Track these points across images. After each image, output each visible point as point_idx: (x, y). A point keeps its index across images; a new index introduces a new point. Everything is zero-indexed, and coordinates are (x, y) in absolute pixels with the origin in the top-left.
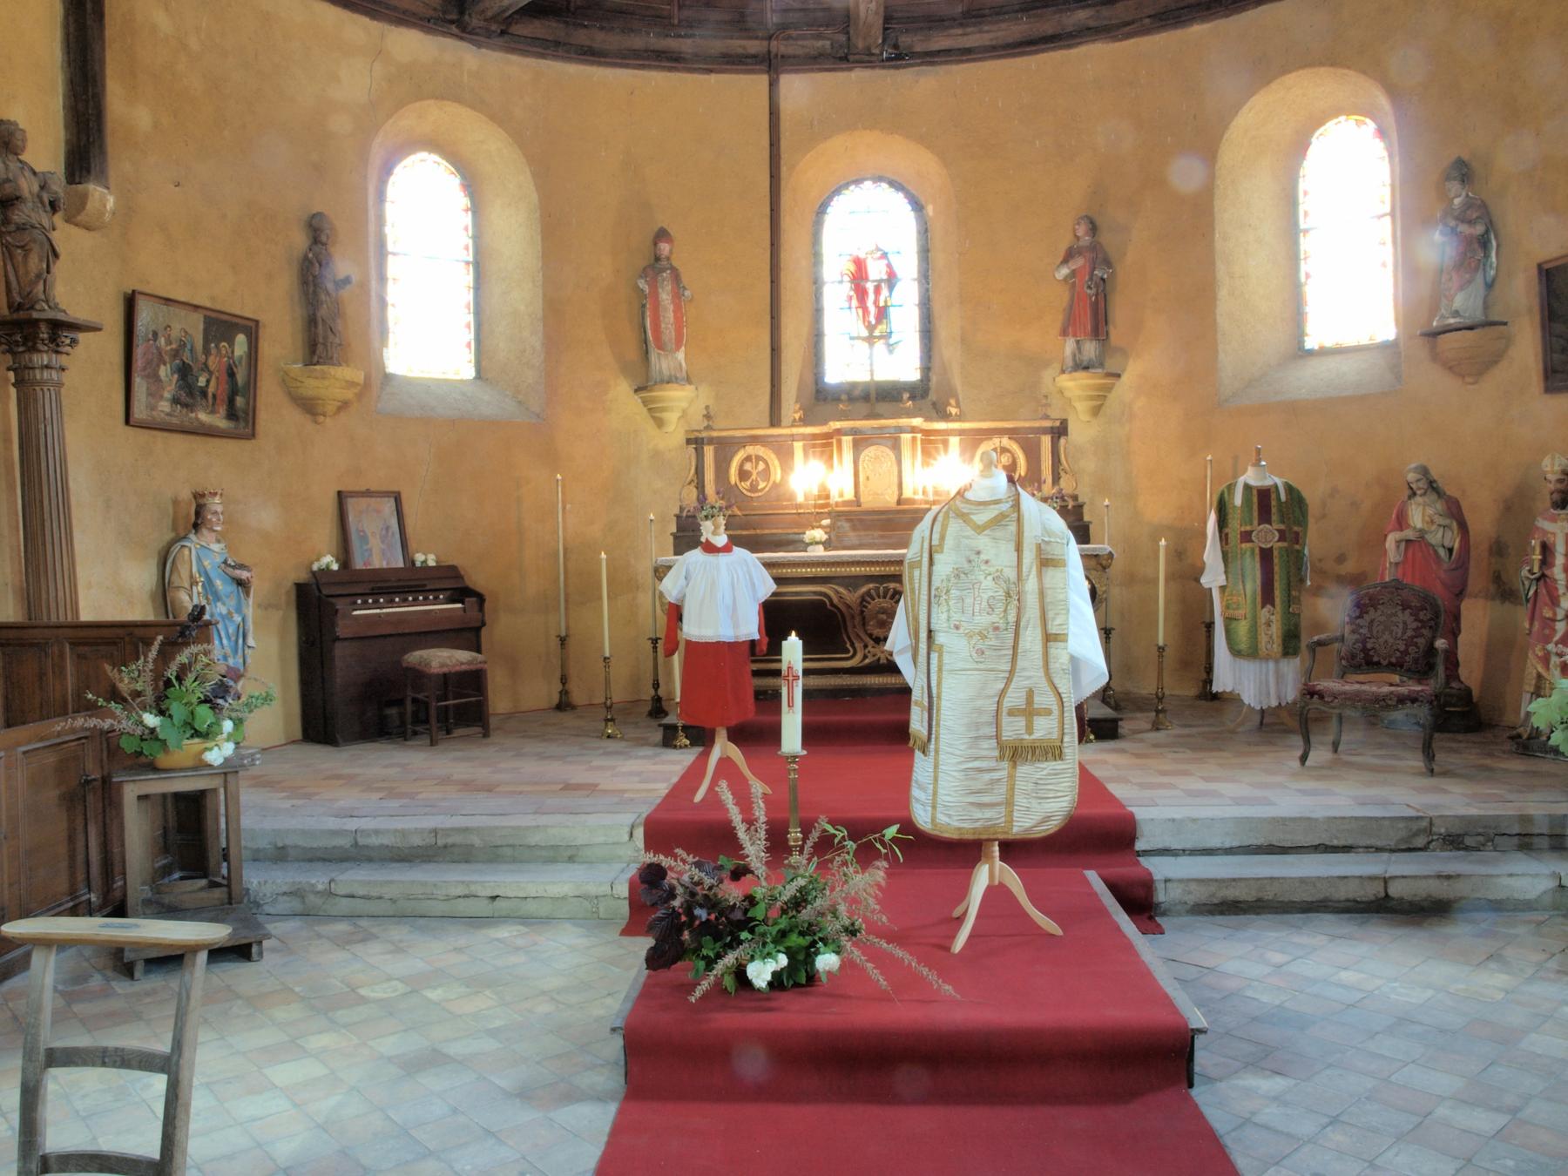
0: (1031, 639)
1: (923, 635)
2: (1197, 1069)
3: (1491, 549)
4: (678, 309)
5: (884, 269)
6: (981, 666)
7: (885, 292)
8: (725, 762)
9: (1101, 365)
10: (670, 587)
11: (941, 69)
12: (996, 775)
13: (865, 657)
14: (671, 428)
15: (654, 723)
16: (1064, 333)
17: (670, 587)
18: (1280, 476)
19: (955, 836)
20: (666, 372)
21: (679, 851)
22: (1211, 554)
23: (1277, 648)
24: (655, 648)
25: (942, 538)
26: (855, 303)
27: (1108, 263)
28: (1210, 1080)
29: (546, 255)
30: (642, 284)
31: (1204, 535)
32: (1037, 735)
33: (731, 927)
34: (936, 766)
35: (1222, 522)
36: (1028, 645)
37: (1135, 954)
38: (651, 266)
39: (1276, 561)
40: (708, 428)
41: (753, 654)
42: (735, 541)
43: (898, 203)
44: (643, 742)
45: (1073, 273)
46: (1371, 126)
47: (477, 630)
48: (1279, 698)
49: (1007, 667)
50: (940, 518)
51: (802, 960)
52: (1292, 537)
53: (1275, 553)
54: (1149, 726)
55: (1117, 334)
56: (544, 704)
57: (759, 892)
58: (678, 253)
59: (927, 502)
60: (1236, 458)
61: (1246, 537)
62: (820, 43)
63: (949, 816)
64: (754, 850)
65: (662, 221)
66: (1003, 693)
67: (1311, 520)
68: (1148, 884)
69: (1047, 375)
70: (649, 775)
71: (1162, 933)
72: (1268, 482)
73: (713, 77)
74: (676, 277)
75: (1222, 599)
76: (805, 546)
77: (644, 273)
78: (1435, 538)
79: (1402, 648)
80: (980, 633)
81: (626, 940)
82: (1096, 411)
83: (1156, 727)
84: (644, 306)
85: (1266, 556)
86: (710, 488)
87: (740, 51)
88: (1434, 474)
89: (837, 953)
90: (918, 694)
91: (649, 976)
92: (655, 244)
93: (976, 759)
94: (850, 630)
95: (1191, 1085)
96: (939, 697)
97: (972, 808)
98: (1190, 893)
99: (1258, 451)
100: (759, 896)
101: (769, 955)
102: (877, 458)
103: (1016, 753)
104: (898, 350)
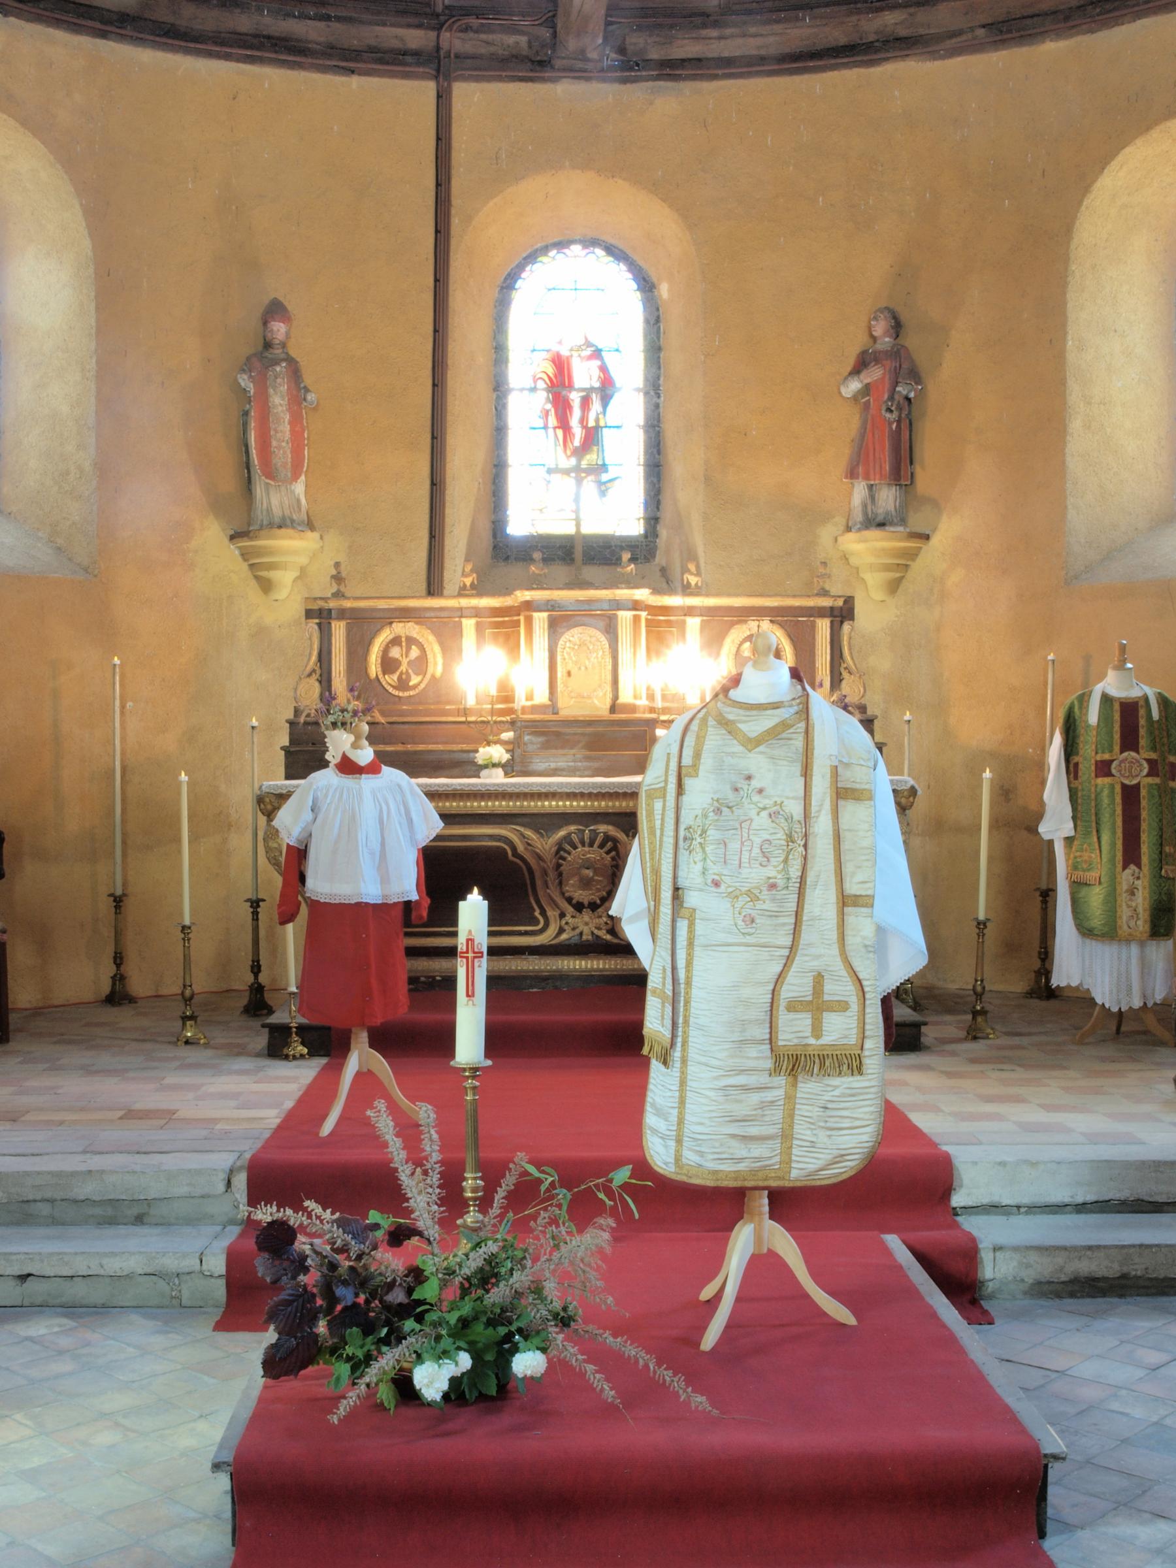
0: (821, 902)
1: (666, 895)
2: (1050, 1512)
4: (296, 420)
5: (596, 373)
6: (749, 939)
7: (596, 406)
8: (364, 1077)
9: (903, 521)
10: (290, 823)
11: (687, 87)
12: (769, 1096)
13: (561, 931)
14: (282, 593)
15: (256, 1023)
16: (852, 474)
17: (290, 823)
18: (1150, 685)
19: (710, 1183)
20: (277, 512)
21: (310, 1204)
23: (1142, 925)
24: (255, 914)
25: (697, 755)
26: (552, 421)
27: (915, 376)
28: (1068, 1527)
29: (102, 330)
30: (244, 381)
31: (1040, 766)
32: (826, 1040)
33: (386, 1314)
34: (683, 1083)
35: (1070, 748)
36: (817, 911)
37: (961, 1351)
38: (260, 356)
39: (1144, 803)
40: (338, 595)
41: (407, 922)
42: (383, 759)
43: (617, 280)
44: (239, 1051)
45: (867, 389)
46: (461, 904)
49: (788, 941)
50: (694, 727)
51: (493, 1360)
53: (1143, 792)
54: (963, 1034)
55: (925, 479)
56: (88, 996)
57: (430, 1264)
58: (297, 336)
59: (652, 710)
60: (1087, 659)
61: (1104, 768)
62: (511, 40)
63: (701, 1154)
64: (422, 1201)
65: (276, 288)
66: (780, 978)
68: (970, 1252)
69: (826, 534)
70: (248, 1099)
71: (991, 1323)
72: (1135, 693)
73: (355, 81)
74: (295, 373)
75: (1067, 854)
76: (476, 769)
77: (247, 366)
80: (749, 893)
81: (223, 1337)
82: (894, 587)
83: (973, 1035)
84: (246, 414)
85: (1130, 795)
86: (339, 683)
87: (396, 44)
89: (544, 1350)
91: (265, 1387)
92: (265, 323)
93: (742, 1072)
94: (541, 893)
95: (1042, 1535)
96: (688, 983)
97: (734, 1143)
98: (1028, 1266)
99: (1123, 648)
100: (429, 1269)
101: (445, 1354)
102: (582, 644)
103: (794, 1064)
104: (614, 490)
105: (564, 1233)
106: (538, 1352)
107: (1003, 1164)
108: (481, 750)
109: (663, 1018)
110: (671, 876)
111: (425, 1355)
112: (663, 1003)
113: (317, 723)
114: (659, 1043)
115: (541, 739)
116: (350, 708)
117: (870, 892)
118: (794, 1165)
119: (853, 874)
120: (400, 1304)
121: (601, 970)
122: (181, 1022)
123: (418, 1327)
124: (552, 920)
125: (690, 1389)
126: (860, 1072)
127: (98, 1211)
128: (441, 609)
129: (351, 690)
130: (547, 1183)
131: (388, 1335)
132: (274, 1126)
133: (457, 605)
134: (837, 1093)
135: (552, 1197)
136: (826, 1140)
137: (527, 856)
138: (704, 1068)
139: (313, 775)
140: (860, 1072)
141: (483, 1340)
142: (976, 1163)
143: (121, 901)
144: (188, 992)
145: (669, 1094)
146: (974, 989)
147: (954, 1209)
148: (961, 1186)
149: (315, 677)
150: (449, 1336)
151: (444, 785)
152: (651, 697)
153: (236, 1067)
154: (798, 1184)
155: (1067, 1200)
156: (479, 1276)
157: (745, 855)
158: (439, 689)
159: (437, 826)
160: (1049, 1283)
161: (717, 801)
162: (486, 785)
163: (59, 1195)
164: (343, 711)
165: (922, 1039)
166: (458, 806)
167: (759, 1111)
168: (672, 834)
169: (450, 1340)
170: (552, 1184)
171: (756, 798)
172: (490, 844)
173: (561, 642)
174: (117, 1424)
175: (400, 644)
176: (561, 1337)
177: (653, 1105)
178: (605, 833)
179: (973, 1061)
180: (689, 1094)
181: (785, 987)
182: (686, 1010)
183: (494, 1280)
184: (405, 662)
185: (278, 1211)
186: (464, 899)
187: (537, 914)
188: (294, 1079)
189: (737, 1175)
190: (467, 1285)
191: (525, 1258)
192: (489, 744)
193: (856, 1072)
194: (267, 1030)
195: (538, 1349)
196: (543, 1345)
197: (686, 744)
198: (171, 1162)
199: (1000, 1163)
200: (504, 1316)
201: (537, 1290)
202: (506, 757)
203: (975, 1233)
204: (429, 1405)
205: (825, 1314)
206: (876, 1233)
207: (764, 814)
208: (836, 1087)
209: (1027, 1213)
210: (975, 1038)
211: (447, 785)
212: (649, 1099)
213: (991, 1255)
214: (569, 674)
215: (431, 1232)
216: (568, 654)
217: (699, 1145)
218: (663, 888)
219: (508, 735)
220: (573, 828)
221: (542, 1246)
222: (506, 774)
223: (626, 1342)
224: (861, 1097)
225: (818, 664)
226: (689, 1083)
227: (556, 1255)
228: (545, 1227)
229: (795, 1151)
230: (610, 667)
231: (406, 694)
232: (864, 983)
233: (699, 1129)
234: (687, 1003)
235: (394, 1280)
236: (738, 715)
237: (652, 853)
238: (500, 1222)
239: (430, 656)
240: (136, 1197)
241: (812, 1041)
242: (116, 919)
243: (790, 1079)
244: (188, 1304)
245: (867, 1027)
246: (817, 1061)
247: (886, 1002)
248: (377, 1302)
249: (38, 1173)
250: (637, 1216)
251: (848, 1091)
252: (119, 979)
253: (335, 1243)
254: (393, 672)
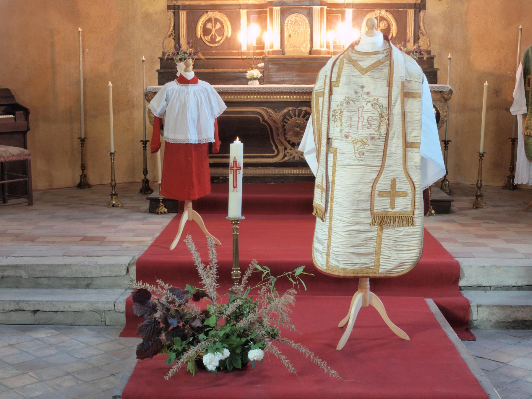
0: (396, 145)
1: (324, 141)
10: (156, 106)
12: (370, 235)
13: (285, 156)
15: (144, 197)
21: (159, 281)
25: (339, 76)
32: (397, 209)
33: (191, 332)
34: (330, 228)
36: (393, 150)
42: (199, 76)
44: (137, 210)
46: (231, 145)
47: (24, 133)
49: (379, 164)
50: (338, 63)
51: (240, 352)
54: (471, 206)
57: (212, 309)
63: (338, 261)
64: (209, 281)
66: (376, 181)
68: (466, 307)
71: (474, 340)
75: (523, 122)
76: (246, 81)
80: (362, 141)
81: (124, 340)
83: (476, 206)
86: (183, 40)
89: (262, 349)
90: (318, 181)
91: (138, 363)
93: (357, 224)
94: (275, 138)
96: (333, 182)
101: (217, 349)
102: (296, 22)
103: (383, 221)
105: (273, 296)
106: (260, 350)
107: (483, 267)
108: (248, 72)
109: (322, 199)
110: (326, 133)
111: (209, 350)
112: (322, 192)
113: (173, 59)
114: (320, 210)
115: (277, 67)
116: (188, 52)
117: (418, 141)
118: (380, 267)
119: (411, 133)
120: (198, 327)
121: (303, 174)
122: (110, 197)
123: (205, 337)
124: (281, 151)
125: (329, 368)
126: (412, 225)
127: (69, 282)
128: (231, 5)
129: (188, 43)
130: (265, 274)
131: (193, 340)
132: (149, 245)
133: (238, 3)
134: (401, 234)
135: (268, 280)
136: (396, 255)
137: (269, 121)
138: (340, 222)
139: (166, 84)
140: (412, 225)
141: (235, 344)
142: (471, 266)
143: (84, 141)
144: (113, 183)
145: (324, 233)
146: (477, 185)
147: (460, 287)
148: (464, 277)
149: (172, 37)
150: (220, 342)
151: (231, 88)
152: (328, 47)
153: (134, 217)
154: (383, 275)
155: (514, 284)
156: (234, 315)
157: (360, 123)
158: (230, 43)
159: (224, 107)
160: (503, 322)
161: (348, 98)
162: (250, 88)
163: (52, 275)
164: (185, 53)
165: (452, 208)
166: (237, 98)
167: (365, 242)
168: (327, 113)
169: (220, 344)
170: (268, 274)
171: (366, 97)
172: (252, 115)
173: (286, 21)
174: (74, 377)
175: (211, 22)
176: (270, 343)
177: (317, 238)
178: (305, 111)
179: (475, 218)
180: (333, 234)
181: (378, 185)
182: (332, 195)
183: (241, 317)
184: (214, 30)
185: (143, 284)
186: (233, 142)
187: (274, 148)
188: (161, 223)
189: (354, 271)
190: (229, 319)
191: (255, 307)
192: (252, 69)
193: (410, 224)
194: (149, 201)
195: (260, 348)
196: (262, 346)
197: (334, 71)
198: (102, 261)
199: (482, 267)
200: (245, 333)
201: (260, 321)
202: (260, 75)
203: (469, 298)
204: (211, 372)
205: (395, 335)
206: (423, 297)
207: (369, 104)
208: (401, 231)
209: (494, 290)
210: (477, 208)
211: (232, 88)
212: (315, 236)
213: (476, 309)
214: (290, 36)
215: (213, 295)
216: (290, 26)
217: (337, 257)
218: (322, 138)
219: (261, 65)
220: (290, 108)
221: (263, 302)
222: (260, 83)
223: (300, 346)
224: (413, 236)
225: (408, 31)
226: (333, 229)
227: (269, 306)
228: (265, 293)
229: (381, 261)
230: (309, 33)
231: (214, 45)
232: (415, 183)
233: (337, 249)
234: (333, 191)
235: (196, 316)
236: (358, 58)
237: (318, 122)
238: (245, 291)
239: (225, 27)
240: (86, 276)
241: (390, 210)
242: (82, 149)
243: (379, 227)
244: (109, 324)
245: (416, 204)
246: (392, 219)
247: (426, 193)
248: (188, 325)
249: (42, 265)
250: (306, 289)
251: (406, 233)
252: (84, 176)
253: (168, 299)
254: (208, 35)
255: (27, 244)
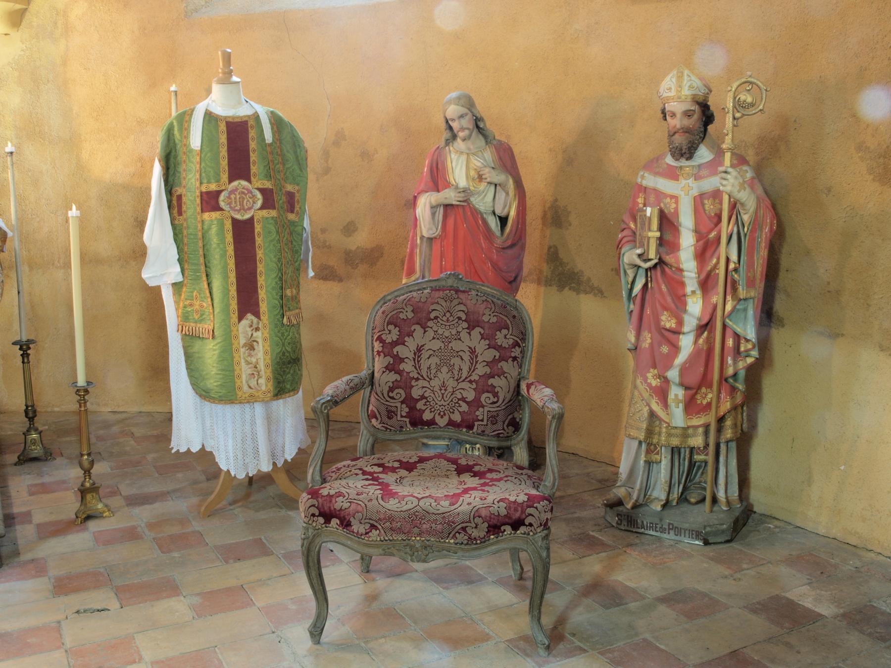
3: (544, 217)
22: (157, 232)
23: (265, 384)
48: (273, 455)
52: (283, 200)
53: (258, 228)
61: (210, 201)
67: (311, 177)
72: (243, 111)
75: (177, 303)
78: (484, 201)
79: (470, 396)
85: (243, 232)
88: (481, 108)
255: (230, 443)
